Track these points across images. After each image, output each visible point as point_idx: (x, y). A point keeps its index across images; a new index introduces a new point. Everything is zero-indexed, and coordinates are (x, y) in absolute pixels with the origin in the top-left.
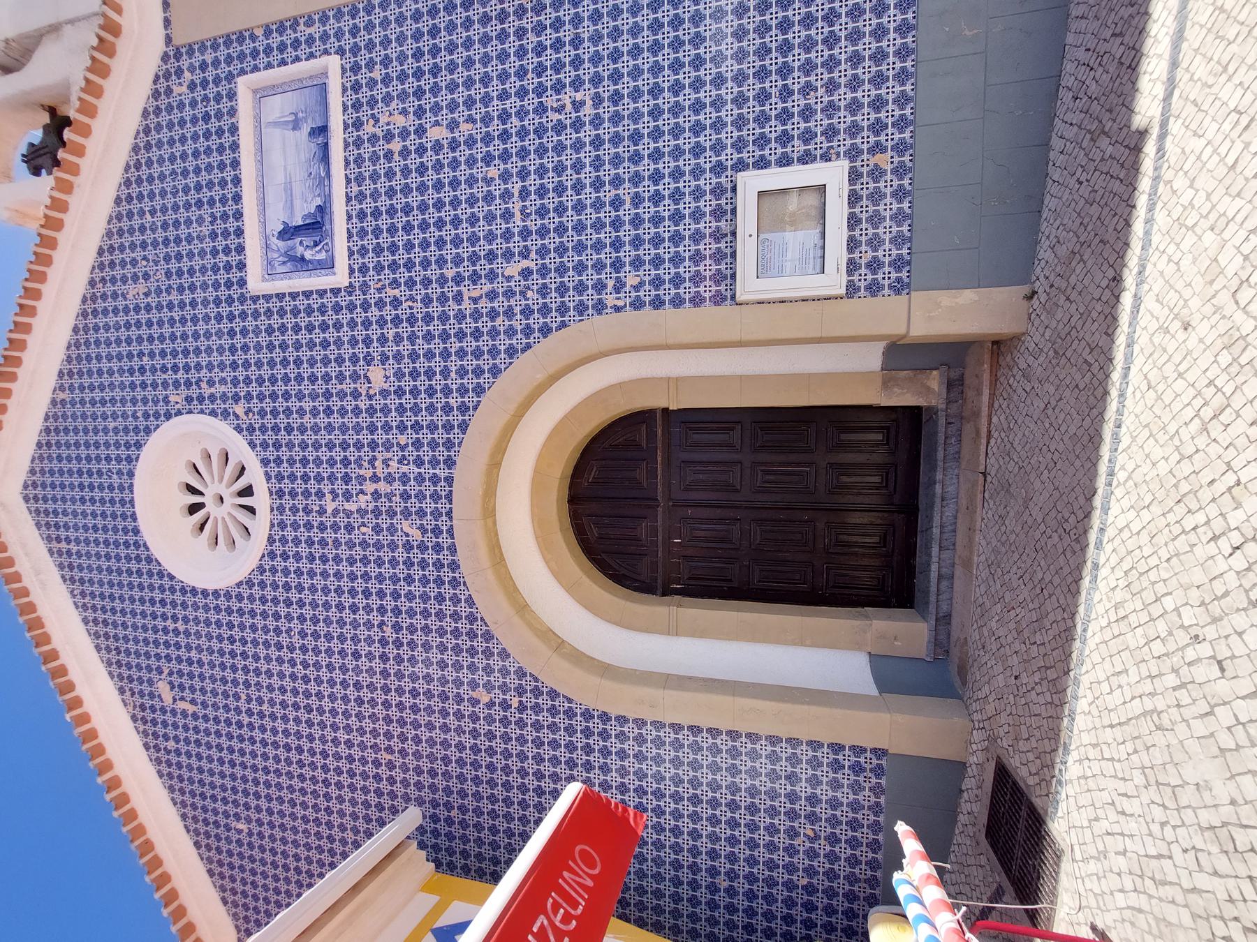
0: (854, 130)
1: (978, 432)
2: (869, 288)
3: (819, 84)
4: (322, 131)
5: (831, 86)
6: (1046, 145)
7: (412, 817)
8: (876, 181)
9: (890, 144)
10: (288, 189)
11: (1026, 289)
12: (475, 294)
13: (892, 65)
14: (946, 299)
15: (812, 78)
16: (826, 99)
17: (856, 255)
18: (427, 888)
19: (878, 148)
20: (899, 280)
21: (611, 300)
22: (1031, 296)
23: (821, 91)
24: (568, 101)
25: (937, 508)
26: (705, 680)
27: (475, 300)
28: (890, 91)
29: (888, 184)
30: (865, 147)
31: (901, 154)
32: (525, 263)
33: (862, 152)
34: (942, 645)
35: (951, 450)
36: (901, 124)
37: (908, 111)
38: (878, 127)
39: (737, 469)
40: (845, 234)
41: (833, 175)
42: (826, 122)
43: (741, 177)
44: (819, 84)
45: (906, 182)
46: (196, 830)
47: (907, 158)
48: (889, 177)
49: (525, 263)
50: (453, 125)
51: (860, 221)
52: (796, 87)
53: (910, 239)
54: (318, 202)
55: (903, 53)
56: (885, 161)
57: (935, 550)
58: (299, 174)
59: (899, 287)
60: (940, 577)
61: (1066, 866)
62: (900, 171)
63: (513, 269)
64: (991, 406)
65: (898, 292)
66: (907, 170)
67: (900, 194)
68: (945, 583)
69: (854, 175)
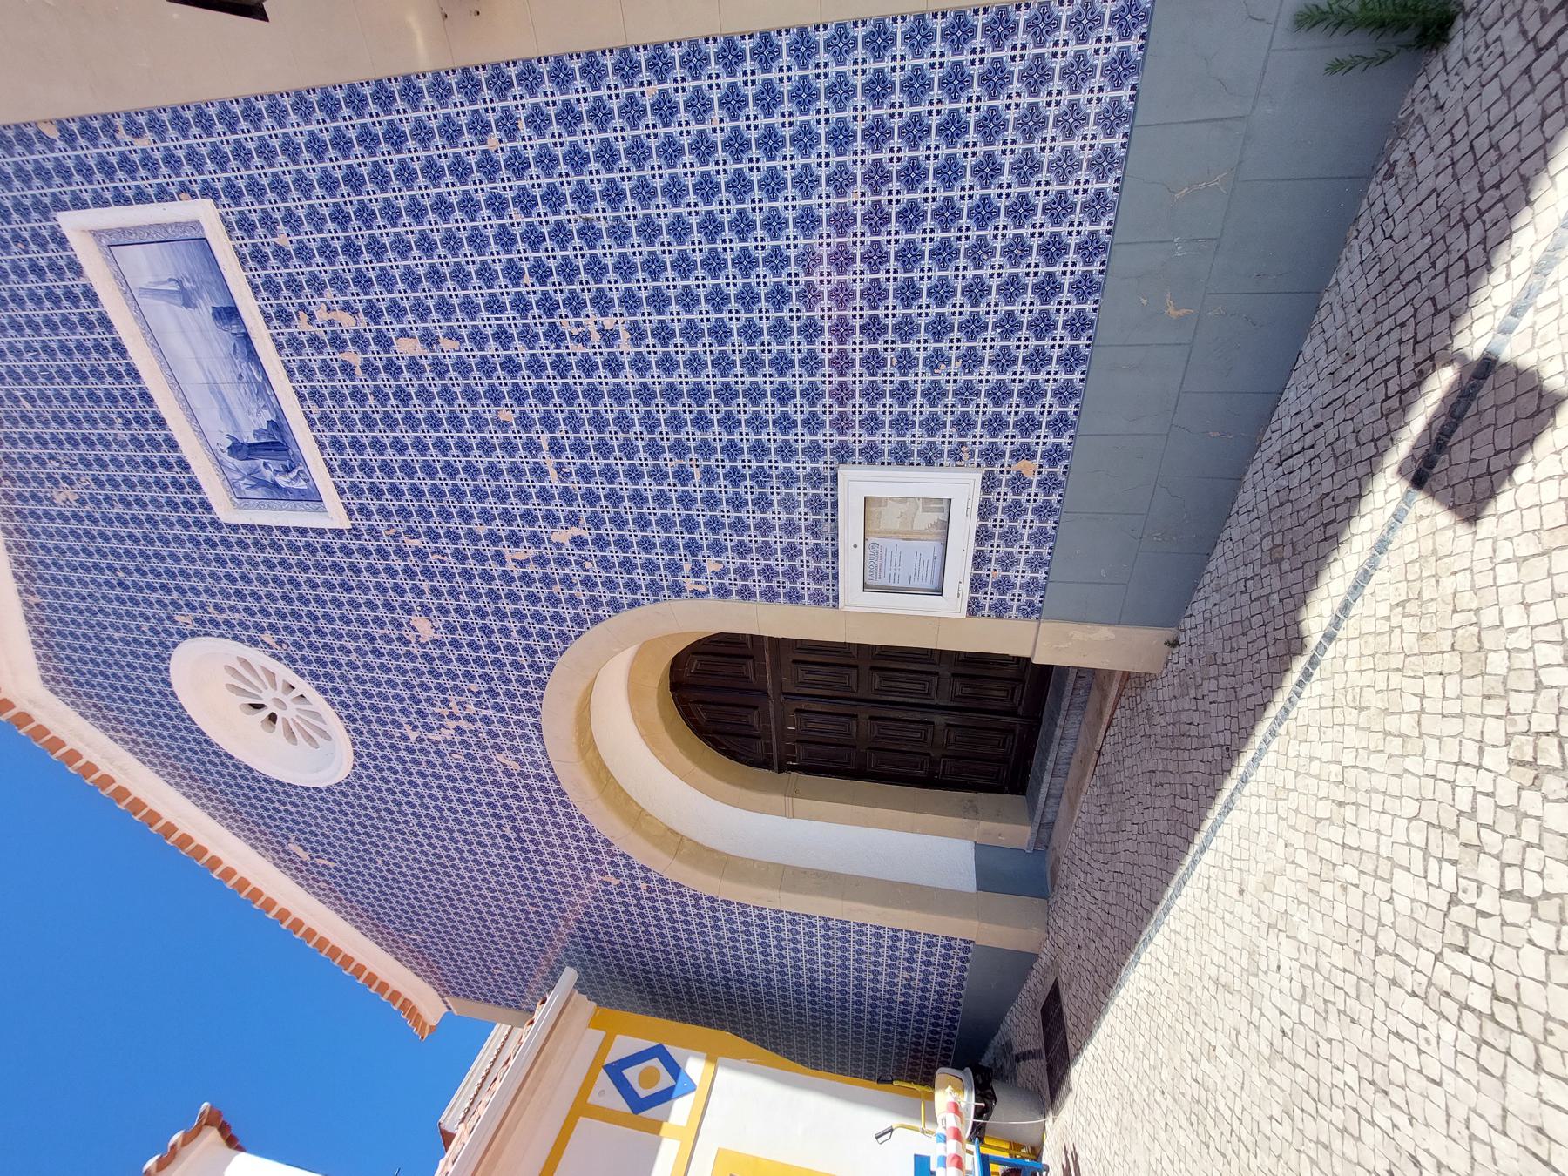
0: (995, 425)
1: (1100, 714)
2: (994, 607)
3: (954, 354)
4: (228, 313)
5: (971, 360)
6: (1239, 480)
7: (569, 975)
8: (1017, 492)
9: (1040, 449)
10: (215, 390)
11: (1169, 634)
12: (521, 556)
13: (1059, 341)
14: (1078, 632)
15: (945, 345)
16: (962, 378)
17: (984, 572)
18: (594, 1023)
19: (1025, 452)
20: (1030, 604)
21: (690, 584)
22: (1175, 644)
23: (955, 366)
24: (593, 329)
25: (1055, 746)
26: (818, 874)
27: (522, 564)
28: (1052, 377)
29: (1031, 498)
30: (1008, 449)
31: (1053, 463)
32: (575, 531)
33: (1003, 454)
34: (1043, 843)
35: (1078, 700)
36: (1071, 359)
37: (1071, 409)
38: (1028, 425)
39: (854, 672)
40: (974, 522)
41: (961, 487)
42: (959, 409)
43: (845, 473)
44: (954, 354)
45: (1054, 498)
46: (311, 673)
47: (1059, 470)
48: (1033, 490)
49: (575, 531)
50: (429, 340)
51: (999, 483)
52: (921, 355)
53: (1049, 563)
54: (268, 416)
55: (1078, 325)
56: (1030, 469)
57: (1047, 778)
58: (225, 376)
59: (1029, 611)
60: (1048, 796)
61: (1070, 1099)
62: (1048, 484)
63: (563, 535)
64: (1119, 696)
65: (1027, 615)
66: (1057, 485)
67: (1043, 511)
68: (1052, 801)
69: (989, 483)
